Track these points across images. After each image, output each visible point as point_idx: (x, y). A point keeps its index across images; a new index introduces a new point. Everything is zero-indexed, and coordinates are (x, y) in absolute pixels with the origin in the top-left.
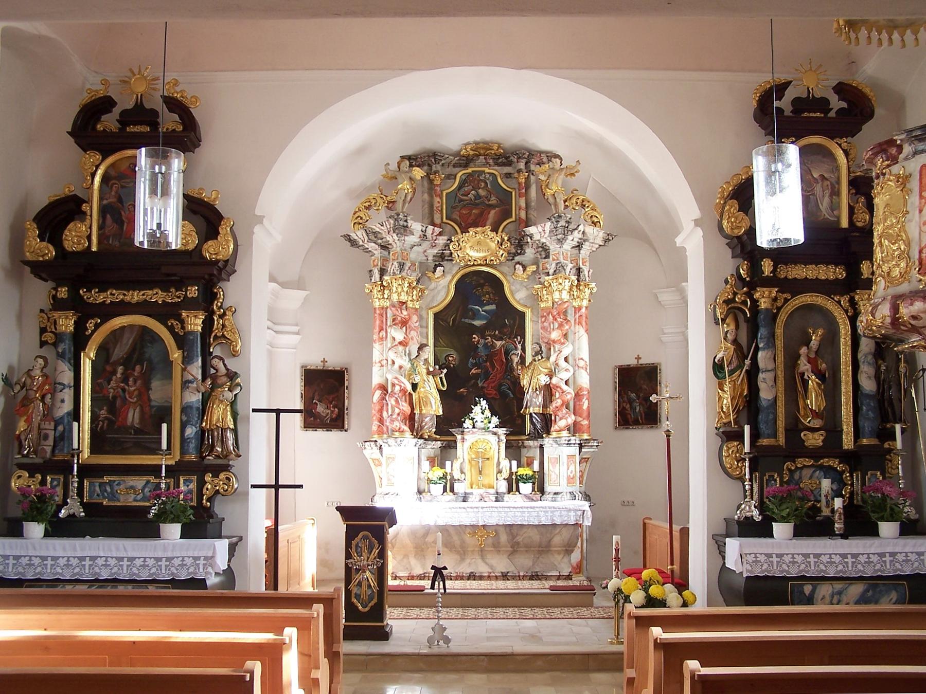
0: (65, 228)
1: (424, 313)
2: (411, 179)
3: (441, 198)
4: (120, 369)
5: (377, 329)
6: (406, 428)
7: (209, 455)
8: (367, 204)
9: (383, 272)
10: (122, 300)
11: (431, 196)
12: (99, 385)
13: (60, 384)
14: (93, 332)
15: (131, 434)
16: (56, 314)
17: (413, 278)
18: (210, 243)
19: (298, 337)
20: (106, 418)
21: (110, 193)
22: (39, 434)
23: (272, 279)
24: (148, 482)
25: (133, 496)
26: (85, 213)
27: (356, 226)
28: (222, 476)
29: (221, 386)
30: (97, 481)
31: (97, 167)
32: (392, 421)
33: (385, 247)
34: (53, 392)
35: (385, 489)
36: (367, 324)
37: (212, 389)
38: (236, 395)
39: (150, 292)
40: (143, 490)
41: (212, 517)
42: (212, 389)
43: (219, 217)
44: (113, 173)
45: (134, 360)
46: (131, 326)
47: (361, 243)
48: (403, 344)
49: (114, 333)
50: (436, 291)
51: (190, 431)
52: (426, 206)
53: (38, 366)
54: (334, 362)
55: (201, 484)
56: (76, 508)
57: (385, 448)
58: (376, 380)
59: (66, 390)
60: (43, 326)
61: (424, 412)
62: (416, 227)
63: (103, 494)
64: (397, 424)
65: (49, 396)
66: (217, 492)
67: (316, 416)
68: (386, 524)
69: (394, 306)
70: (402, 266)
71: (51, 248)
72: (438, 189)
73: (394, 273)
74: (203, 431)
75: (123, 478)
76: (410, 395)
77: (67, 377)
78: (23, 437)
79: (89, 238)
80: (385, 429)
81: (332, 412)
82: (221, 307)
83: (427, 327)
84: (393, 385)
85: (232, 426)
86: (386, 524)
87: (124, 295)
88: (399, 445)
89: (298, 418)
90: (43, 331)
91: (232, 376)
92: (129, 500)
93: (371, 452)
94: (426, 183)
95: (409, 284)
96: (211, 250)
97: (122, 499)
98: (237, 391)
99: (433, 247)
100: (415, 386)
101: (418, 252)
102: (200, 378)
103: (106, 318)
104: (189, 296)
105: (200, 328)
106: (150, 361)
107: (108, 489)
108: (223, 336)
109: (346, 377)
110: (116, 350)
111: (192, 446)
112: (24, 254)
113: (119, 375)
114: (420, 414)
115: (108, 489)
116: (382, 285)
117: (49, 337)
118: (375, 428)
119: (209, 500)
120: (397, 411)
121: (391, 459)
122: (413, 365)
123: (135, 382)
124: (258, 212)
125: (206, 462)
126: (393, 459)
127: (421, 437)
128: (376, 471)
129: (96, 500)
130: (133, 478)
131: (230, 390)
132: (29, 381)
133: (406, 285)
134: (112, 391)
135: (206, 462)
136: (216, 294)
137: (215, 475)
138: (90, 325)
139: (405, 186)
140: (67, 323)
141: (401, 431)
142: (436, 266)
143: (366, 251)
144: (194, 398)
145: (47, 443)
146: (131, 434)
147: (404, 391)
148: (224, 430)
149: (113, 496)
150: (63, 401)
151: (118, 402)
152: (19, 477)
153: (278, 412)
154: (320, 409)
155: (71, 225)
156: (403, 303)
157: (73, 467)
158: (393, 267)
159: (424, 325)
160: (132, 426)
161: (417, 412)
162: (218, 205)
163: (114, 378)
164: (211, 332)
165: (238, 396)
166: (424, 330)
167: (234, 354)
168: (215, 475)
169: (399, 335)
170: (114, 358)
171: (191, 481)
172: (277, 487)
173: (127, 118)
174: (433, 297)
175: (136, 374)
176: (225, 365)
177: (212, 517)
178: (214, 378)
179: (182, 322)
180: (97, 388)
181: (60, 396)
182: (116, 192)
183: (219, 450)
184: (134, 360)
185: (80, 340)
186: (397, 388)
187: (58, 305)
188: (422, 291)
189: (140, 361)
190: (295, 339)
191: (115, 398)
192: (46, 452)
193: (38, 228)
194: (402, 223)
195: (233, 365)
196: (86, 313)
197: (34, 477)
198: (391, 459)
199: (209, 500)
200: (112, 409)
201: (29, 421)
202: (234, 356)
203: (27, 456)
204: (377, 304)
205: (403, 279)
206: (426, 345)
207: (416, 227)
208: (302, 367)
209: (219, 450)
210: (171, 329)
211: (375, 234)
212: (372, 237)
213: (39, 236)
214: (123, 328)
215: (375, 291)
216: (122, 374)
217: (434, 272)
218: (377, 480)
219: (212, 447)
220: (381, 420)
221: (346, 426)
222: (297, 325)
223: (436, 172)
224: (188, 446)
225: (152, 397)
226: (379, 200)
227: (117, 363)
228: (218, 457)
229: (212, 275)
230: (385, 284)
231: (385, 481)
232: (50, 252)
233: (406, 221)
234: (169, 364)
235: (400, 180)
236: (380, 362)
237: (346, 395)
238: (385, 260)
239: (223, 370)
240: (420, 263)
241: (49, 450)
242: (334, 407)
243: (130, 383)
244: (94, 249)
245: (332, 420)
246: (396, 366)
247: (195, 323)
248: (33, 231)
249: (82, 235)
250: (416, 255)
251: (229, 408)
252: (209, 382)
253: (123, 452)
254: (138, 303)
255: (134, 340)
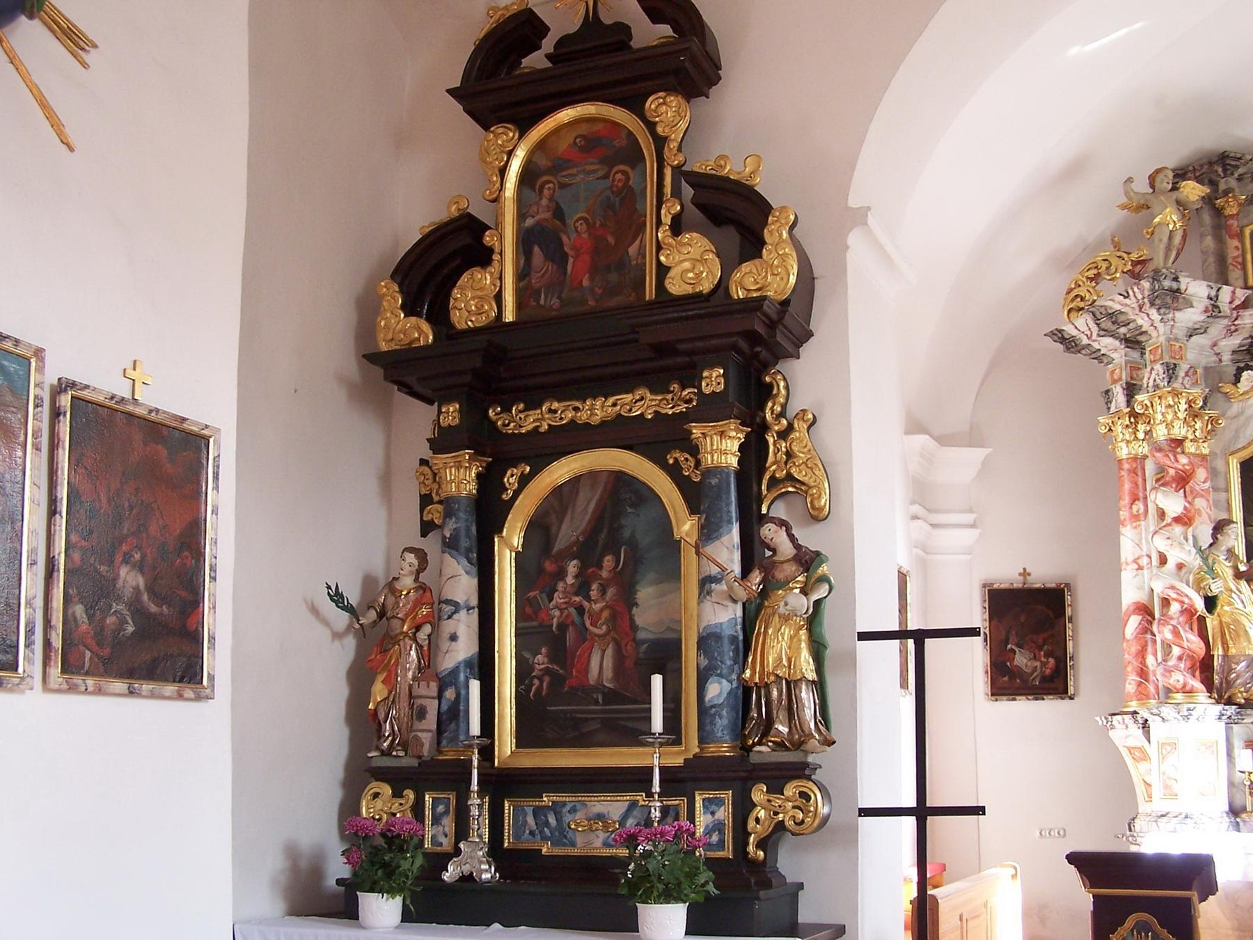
0: (454, 285)
1: (1219, 464)
2: (1178, 203)
3: (1242, 242)
4: (572, 567)
5: (1127, 500)
6: (1197, 684)
7: (760, 743)
8: (1091, 274)
9: (1131, 390)
10: (572, 421)
11: (1219, 240)
12: (532, 602)
13: (448, 602)
14: (517, 494)
15: (596, 702)
16: (439, 460)
17: (1197, 392)
18: (746, 267)
19: (975, 533)
20: (547, 671)
21: (538, 204)
22: (411, 707)
23: (915, 426)
24: (634, 804)
25: (602, 835)
26: (490, 251)
27: (1073, 315)
28: (791, 790)
29: (784, 585)
30: (529, 804)
31: (510, 154)
32: (1169, 671)
33: (1133, 342)
34: (435, 621)
35: (1159, 806)
36: (1107, 491)
37: (764, 594)
38: (818, 603)
39: (628, 398)
40: (622, 822)
41: (767, 884)
42: (764, 594)
43: (763, 208)
44: (542, 162)
45: (601, 543)
46: (593, 475)
47: (1085, 341)
48: (1184, 520)
49: (558, 491)
50: (1242, 418)
51: (717, 690)
52: (1211, 259)
53: (407, 569)
54: (1043, 573)
55: (743, 808)
56: (476, 863)
57: (1154, 724)
58: (1130, 594)
59: (462, 614)
60: (424, 492)
61: (1233, 651)
62: (1197, 290)
63: (541, 832)
64: (1178, 678)
65: (427, 629)
66: (781, 826)
67: (1014, 673)
68: (1194, 895)
69: (1160, 450)
70: (1171, 371)
71: (426, 327)
72: (1234, 223)
73: (1156, 387)
74: (746, 690)
75: (582, 797)
76: (1202, 620)
77: (464, 586)
78: (381, 716)
79: (499, 298)
80: (1151, 688)
81: (1044, 664)
82: (782, 414)
83: (1227, 490)
84: (1166, 602)
85: (811, 675)
86: (1194, 895)
87: (576, 409)
88: (1187, 718)
89: (975, 653)
90: (426, 500)
91: (808, 560)
92: (595, 844)
93: (1125, 734)
94: (1207, 217)
95: (1189, 402)
96: (747, 281)
97: (580, 840)
98: (821, 592)
99: (1230, 332)
100: (1211, 603)
101: (1202, 347)
102: (737, 569)
103: (541, 461)
104: (707, 391)
105: (734, 461)
106: (633, 544)
107: (552, 820)
108: (790, 478)
109: (1068, 599)
110: (564, 527)
111: (722, 723)
112: (377, 345)
113: (570, 580)
114: (1225, 656)
115: (552, 820)
116: (1133, 414)
117: (435, 513)
118: (1130, 688)
119: (761, 844)
120: (1176, 651)
121: (1171, 746)
122: (1205, 559)
123: (603, 591)
124: (854, 201)
125: (754, 758)
126: (1174, 746)
127: (1229, 702)
128: (1137, 771)
129: (527, 844)
130: (602, 796)
131: (804, 592)
132: (391, 600)
133: (1183, 406)
134: (557, 613)
135: (754, 758)
136: (770, 386)
137: (776, 788)
138: (511, 479)
139: (1169, 218)
140: (461, 477)
141: (1188, 691)
142: (1239, 372)
143: (1099, 357)
144: (724, 615)
145: (424, 725)
146: (596, 702)
147: (1189, 612)
148: (792, 685)
149: (562, 835)
150: (454, 638)
151: (570, 635)
152: (376, 795)
153: (920, 637)
154: (1021, 660)
155: (465, 278)
156: (1179, 442)
157: (471, 774)
158: (1153, 374)
159: (1222, 484)
160: (599, 687)
161: (1218, 652)
162: (763, 186)
163: (560, 586)
164: (762, 469)
165: (827, 608)
166: (1223, 495)
167: (816, 517)
168: (776, 788)
169: (1173, 504)
170: (559, 545)
171: (720, 802)
172: (922, 812)
173: (566, 50)
174: (1237, 431)
175: (604, 574)
176: (792, 537)
177: (767, 884)
178: (768, 569)
179: (694, 450)
180: (528, 610)
181: (448, 627)
182: (551, 199)
183: (784, 729)
184: (601, 543)
185: (489, 511)
186: (1175, 608)
187: (443, 442)
188: (1213, 421)
189: (612, 547)
190: (968, 536)
191: (563, 627)
192: (422, 745)
193: (401, 291)
194: (1167, 283)
195: (810, 538)
196: (501, 455)
197: (401, 796)
198: (1171, 746)
199: (761, 844)
200: (559, 653)
201: (390, 682)
202: (816, 519)
203: (386, 753)
204: (1123, 452)
205: (1176, 394)
206: (1229, 522)
207: (1197, 290)
208: (984, 586)
209: (784, 729)
210: (674, 472)
211: (1113, 316)
212: (1107, 324)
213: (403, 307)
214: (575, 481)
215: (1118, 429)
216: (576, 577)
217: (1237, 379)
218: (1140, 789)
219: (769, 723)
220: (1143, 673)
221: (1071, 690)
222: (971, 511)
223: (1226, 193)
224: (712, 723)
225: (639, 621)
226: (1114, 261)
227: (567, 555)
228: (780, 746)
229: (753, 337)
230: (1138, 409)
231: (1157, 791)
232: (422, 332)
233: (1176, 279)
234: (672, 546)
235: (1156, 207)
236: (1135, 561)
237: (1069, 632)
238: (1134, 368)
239: (786, 549)
240: (1206, 369)
241: (427, 739)
242: (1047, 655)
243: (594, 593)
244: (509, 317)
245: (1044, 679)
246: (1171, 564)
247: (723, 448)
248: (393, 297)
249: (487, 297)
250: (1196, 352)
251: (803, 634)
252: (756, 577)
253: (582, 740)
254: (603, 423)
255: (600, 500)
